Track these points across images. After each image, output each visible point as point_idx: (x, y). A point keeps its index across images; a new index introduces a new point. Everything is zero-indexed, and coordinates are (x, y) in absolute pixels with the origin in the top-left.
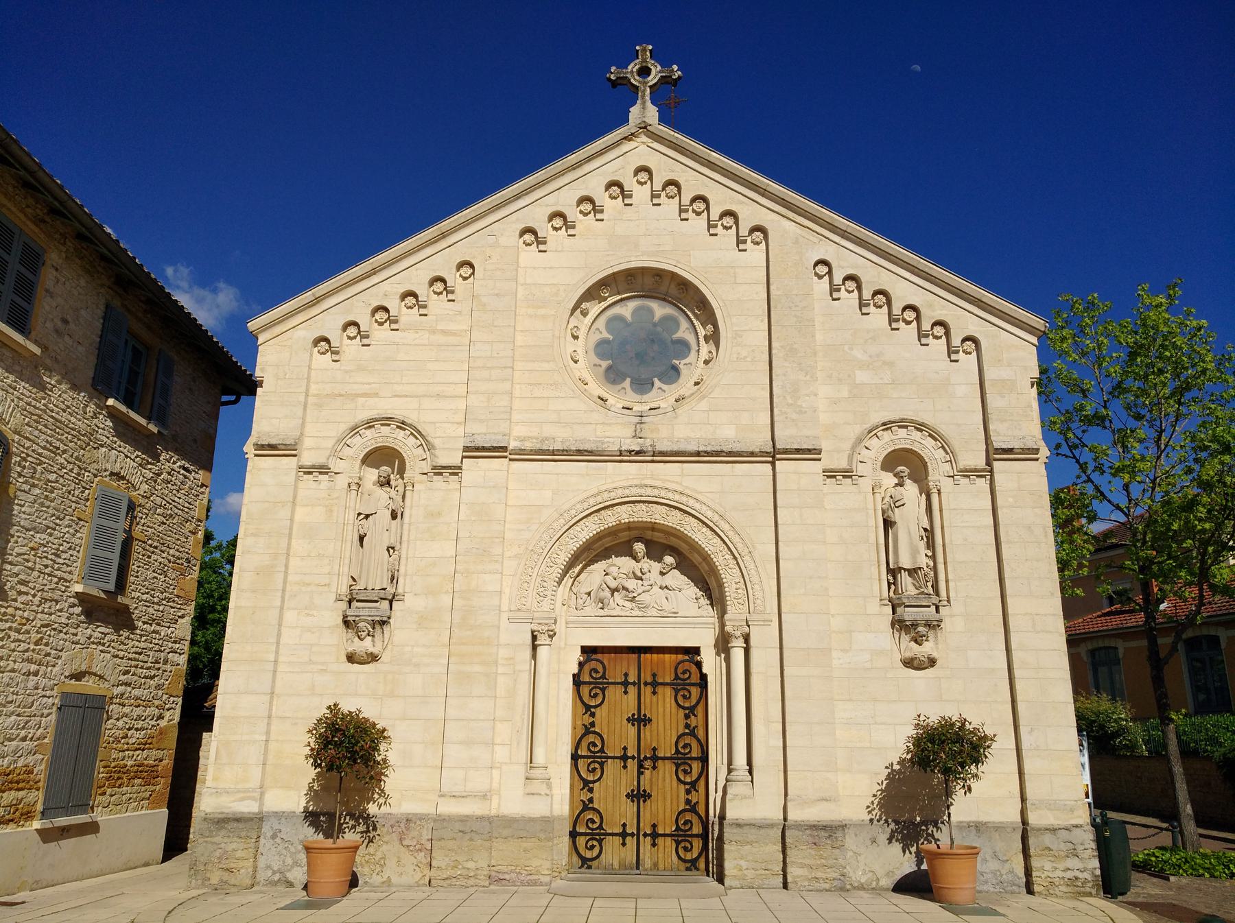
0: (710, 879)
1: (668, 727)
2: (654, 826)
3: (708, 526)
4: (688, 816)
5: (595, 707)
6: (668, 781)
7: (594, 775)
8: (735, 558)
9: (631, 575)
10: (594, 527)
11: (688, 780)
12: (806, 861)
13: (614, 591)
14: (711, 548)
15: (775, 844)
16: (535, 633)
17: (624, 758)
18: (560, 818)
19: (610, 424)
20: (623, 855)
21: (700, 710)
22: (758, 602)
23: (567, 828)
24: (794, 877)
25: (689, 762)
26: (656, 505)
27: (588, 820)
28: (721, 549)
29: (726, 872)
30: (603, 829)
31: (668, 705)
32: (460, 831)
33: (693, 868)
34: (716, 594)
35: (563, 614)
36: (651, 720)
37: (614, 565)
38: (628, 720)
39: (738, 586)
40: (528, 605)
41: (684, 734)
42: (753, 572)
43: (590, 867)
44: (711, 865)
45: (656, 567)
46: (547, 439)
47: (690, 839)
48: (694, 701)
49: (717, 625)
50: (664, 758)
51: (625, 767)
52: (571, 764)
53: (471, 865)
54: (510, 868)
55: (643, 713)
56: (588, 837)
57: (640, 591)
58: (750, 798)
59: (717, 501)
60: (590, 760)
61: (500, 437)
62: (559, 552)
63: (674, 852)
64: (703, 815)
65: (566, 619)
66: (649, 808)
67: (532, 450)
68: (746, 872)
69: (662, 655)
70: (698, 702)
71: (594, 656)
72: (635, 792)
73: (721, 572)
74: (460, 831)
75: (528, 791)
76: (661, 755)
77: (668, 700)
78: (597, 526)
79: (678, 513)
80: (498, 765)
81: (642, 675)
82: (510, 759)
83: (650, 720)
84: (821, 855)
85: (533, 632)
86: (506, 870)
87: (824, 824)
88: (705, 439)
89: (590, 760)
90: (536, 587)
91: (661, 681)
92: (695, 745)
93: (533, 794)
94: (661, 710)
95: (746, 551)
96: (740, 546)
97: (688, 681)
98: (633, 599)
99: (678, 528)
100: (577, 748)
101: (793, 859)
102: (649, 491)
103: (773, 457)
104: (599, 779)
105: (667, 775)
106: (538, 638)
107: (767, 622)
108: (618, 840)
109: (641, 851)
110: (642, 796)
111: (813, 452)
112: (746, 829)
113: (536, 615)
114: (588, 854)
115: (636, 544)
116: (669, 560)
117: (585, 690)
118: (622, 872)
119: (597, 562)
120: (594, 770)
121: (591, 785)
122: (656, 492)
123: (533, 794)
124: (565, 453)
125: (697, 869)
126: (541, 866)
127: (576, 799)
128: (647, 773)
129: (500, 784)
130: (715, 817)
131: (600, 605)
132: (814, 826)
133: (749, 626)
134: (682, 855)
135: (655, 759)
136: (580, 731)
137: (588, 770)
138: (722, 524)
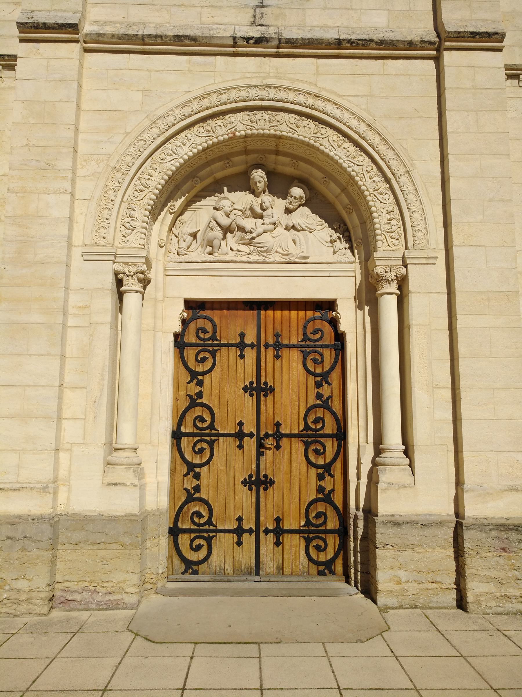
0: (352, 589)
1: (294, 396)
2: (278, 520)
3: (351, 139)
4: (321, 507)
5: (204, 374)
6: (295, 464)
7: (201, 458)
8: (387, 180)
9: (248, 212)
10: (199, 140)
11: (321, 462)
12: (493, 574)
13: (227, 230)
14: (356, 168)
15: (444, 548)
16: (121, 276)
17: (240, 436)
18: (157, 513)
19: (220, 7)
20: (238, 557)
21: (335, 376)
22: (419, 234)
23: (166, 524)
24: (477, 595)
25: (322, 440)
26: (281, 114)
27: (193, 514)
28: (369, 169)
29: (380, 586)
30: (213, 525)
31: (295, 372)
32: (8, 538)
33: (327, 571)
34: (357, 233)
35: (161, 258)
36: (274, 389)
37: (227, 198)
38: (245, 389)
39: (391, 216)
40: (110, 238)
41: (315, 406)
42: (411, 197)
43: (195, 573)
44: (352, 571)
45: (280, 204)
46: (134, 24)
47: (323, 536)
48: (327, 366)
49: (359, 272)
50: (290, 436)
51: (241, 447)
52: (172, 444)
53: (23, 584)
54: (82, 585)
55: (263, 380)
56: (193, 535)
57: (260, 229)
58: (408, 487)
59: (363, 107)
60: (196, 439)
61: (69, 15)
62: (152, 172)
63: (303, 552)
64: (340, 505)
65: (164, 265)
66: (271, 497)
67: (113, 36)
68: (406, 586)
69: (287, 312)
70: (332, 368)
71: (202, 313)
72: (254, 478)
73: (369, 198)
74: (8, 538)
75: (108, 480)
76: (286, 431)
77: (294, 365)
78: (203, 139)
79: (312, 124)
80: (68, 446)
81: (263, 335)
82: (84, 439)
83: (272, 390)
84: (513, 565)
85: (116, 274)
86: (75, 588)
87: (516, 522)
88: (348, 28)
89: (196, 439)
90: (120, 217)
91: (285, 342)
92: (328, 419)
93: (115, 484)
94: (286, 377)
95: (403, 170)
96: (394, 164)
97: (320, 343)
98: (250, 242)
99: (312, 142)
100: (180, 422)
101: (474, 571)
102: (272, 93)
103: (438, 50)
104: (208, 462)
105: (294, 457)
106: (125, 282)
107: (430, 260)
108: (232, 538)
109: (262, 552)
110: (263, 483)
111: (494, 37)
112: (406, 529)
113: (120, 252)
114: (194, 557)
115: (255, 171)
116: (297, 192)
117: (190, 354)
118: (236, 578)
119: (205, 197)
120: (201, 450)
121: (197, 470)
122: (282, 95)
123: (115, 484)
124: (159, 40)
125: (333, 573)
126: (125, 581)
127: (179, 488)
128: (269, 454)
129: (70, 472)
130: (357, 509)
131: (209, 249)
132: (503, 525)
133: (406, 267)
134: (314, 556)
135: (278, 436)
136: (184, 403)
137: (194, 451)
138: (370, 135)
